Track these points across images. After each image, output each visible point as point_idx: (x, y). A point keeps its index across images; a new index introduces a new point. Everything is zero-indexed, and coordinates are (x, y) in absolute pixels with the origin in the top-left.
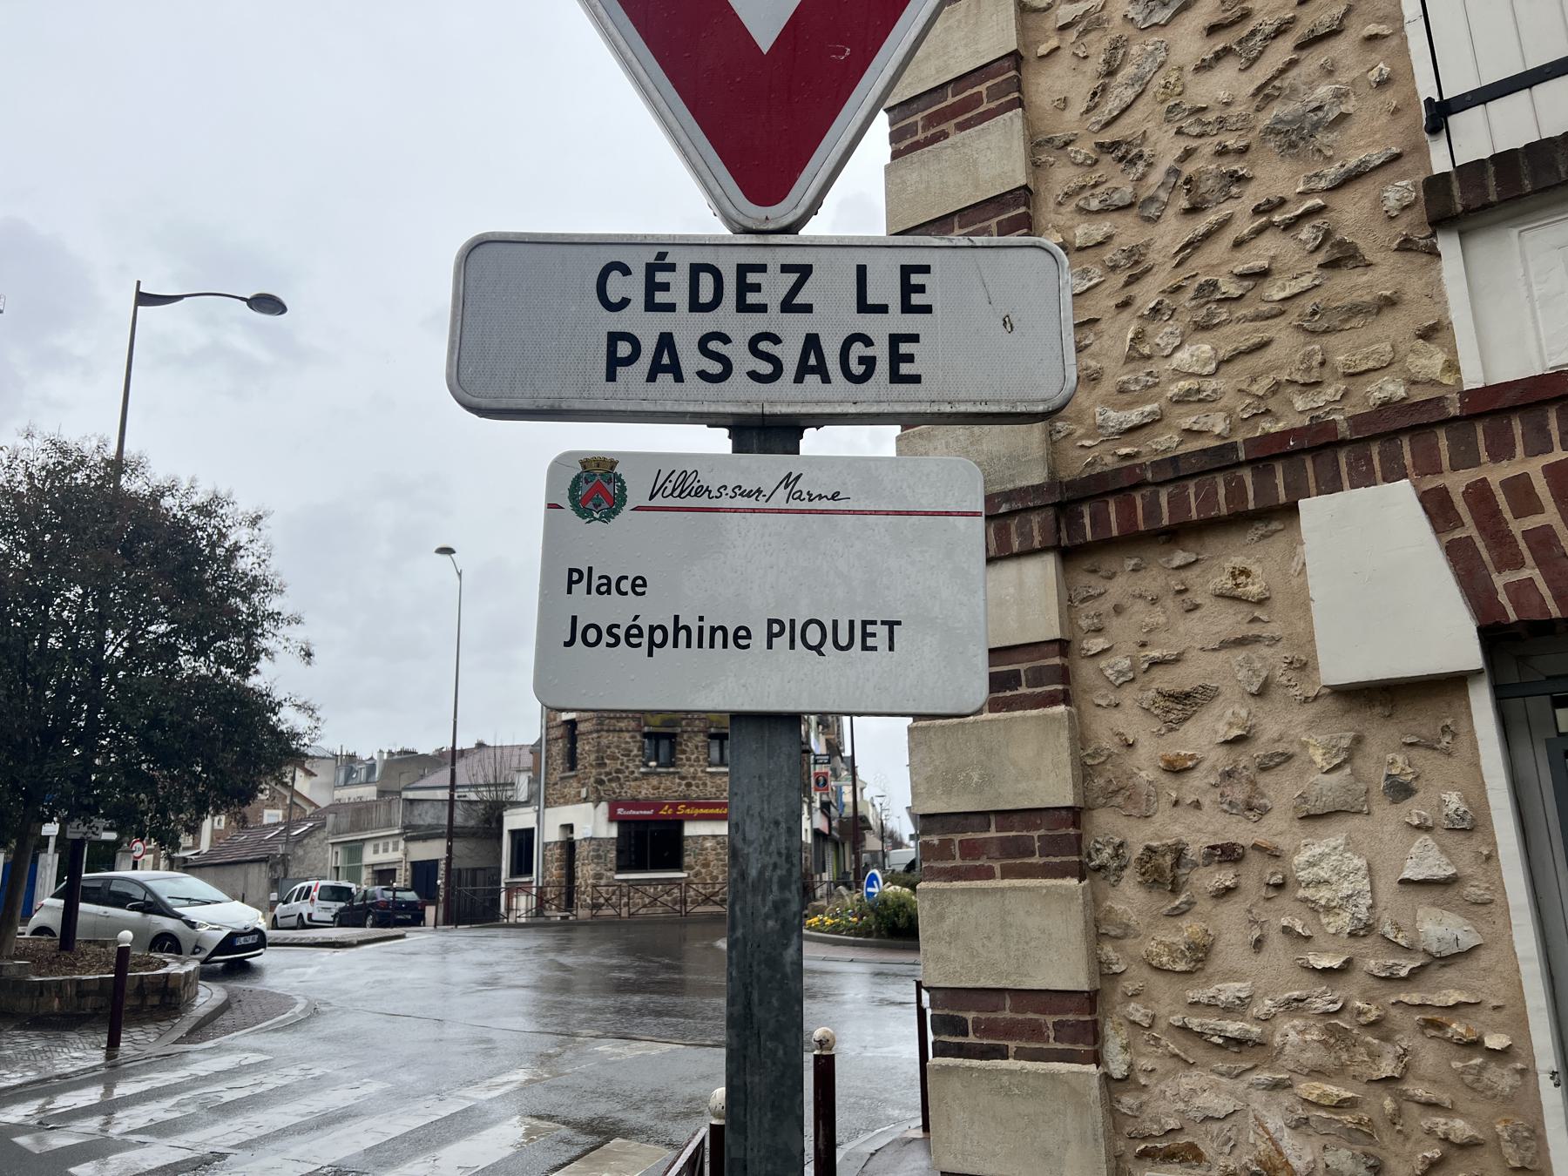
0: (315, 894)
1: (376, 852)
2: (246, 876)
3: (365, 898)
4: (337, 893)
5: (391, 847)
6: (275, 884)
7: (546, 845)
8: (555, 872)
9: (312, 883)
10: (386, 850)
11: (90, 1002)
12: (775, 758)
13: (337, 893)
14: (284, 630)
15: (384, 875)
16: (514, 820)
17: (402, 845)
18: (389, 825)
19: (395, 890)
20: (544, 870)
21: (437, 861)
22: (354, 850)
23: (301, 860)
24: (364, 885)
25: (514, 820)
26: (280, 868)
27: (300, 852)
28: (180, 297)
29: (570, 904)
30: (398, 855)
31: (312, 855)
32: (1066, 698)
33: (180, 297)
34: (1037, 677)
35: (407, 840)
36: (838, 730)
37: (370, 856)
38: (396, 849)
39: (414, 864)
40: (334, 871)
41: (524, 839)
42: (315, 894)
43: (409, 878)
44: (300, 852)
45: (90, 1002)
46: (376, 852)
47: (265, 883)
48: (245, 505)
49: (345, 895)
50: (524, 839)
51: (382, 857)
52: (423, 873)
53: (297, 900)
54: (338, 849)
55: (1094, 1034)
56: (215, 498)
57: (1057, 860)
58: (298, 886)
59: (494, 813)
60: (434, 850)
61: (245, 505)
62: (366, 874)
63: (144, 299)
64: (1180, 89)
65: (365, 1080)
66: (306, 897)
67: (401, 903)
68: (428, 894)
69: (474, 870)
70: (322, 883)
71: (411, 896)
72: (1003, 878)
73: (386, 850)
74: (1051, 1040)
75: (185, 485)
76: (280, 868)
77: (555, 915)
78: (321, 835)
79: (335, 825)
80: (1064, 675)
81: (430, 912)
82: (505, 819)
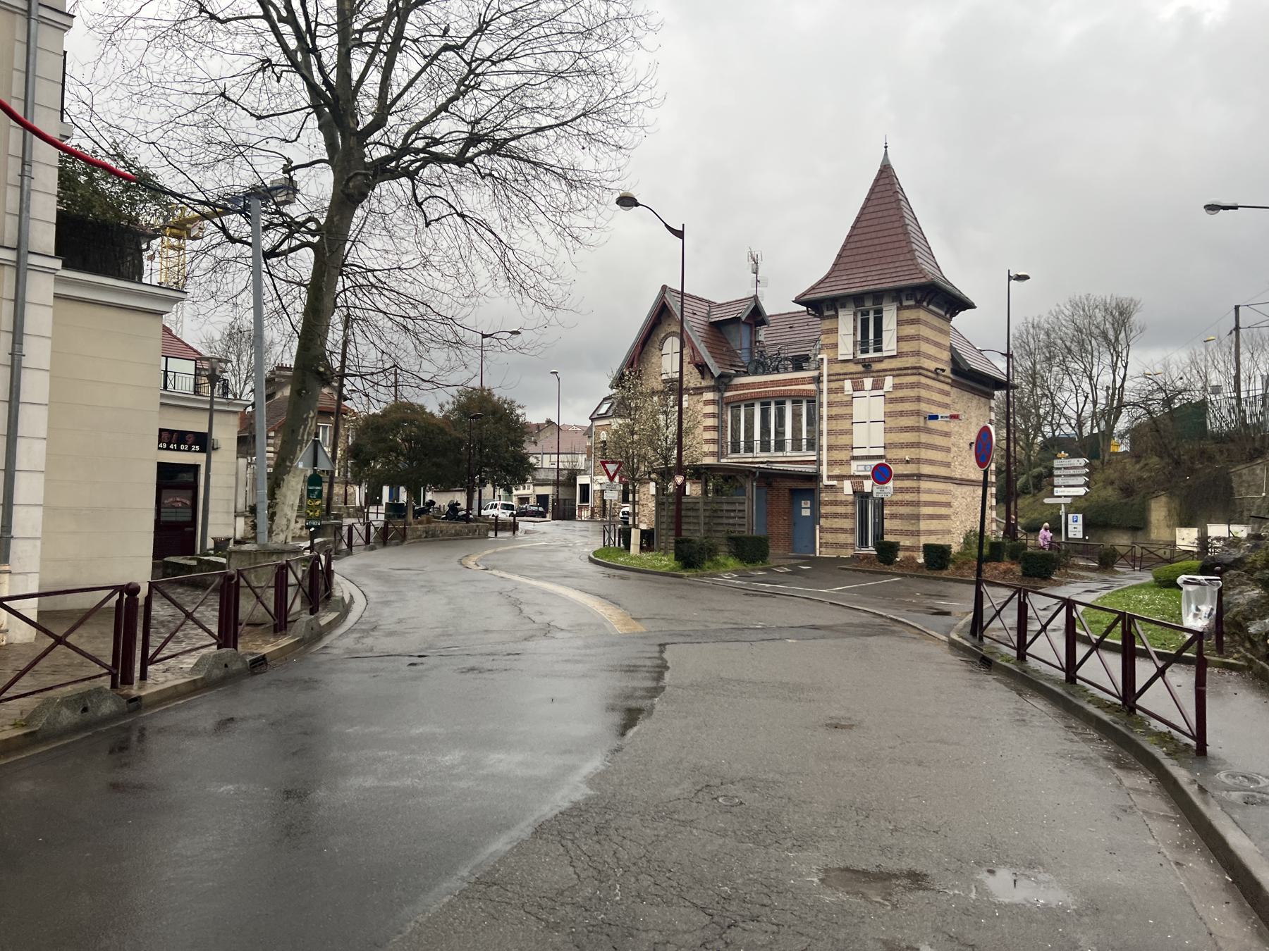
0: (499, 507)
1: (524, 489)
7: (595, 491)
8: (598, 502)
12: (149, 216)
16: (582, 480)
17: (532, 487)
20: (594, 501)
21: (548, 495)
25: (582, 480)
29: (604, 515)
30: (530, 491)
32: (780, 404)
35: (534, 485)
38: (529, 489)
39: (537, 496)
41: (585, 488)
42: (499, 507)
50: (585, 488)
52: (542, 499)
57: (742, 438)
59: (573, 474)
60: (547, 490)
62: (515, 499)
65: (549, 565)
66: (495, 507)
69: (565, 500)
72: (862, 319)
74: (742, 451)
77: (598, 517)
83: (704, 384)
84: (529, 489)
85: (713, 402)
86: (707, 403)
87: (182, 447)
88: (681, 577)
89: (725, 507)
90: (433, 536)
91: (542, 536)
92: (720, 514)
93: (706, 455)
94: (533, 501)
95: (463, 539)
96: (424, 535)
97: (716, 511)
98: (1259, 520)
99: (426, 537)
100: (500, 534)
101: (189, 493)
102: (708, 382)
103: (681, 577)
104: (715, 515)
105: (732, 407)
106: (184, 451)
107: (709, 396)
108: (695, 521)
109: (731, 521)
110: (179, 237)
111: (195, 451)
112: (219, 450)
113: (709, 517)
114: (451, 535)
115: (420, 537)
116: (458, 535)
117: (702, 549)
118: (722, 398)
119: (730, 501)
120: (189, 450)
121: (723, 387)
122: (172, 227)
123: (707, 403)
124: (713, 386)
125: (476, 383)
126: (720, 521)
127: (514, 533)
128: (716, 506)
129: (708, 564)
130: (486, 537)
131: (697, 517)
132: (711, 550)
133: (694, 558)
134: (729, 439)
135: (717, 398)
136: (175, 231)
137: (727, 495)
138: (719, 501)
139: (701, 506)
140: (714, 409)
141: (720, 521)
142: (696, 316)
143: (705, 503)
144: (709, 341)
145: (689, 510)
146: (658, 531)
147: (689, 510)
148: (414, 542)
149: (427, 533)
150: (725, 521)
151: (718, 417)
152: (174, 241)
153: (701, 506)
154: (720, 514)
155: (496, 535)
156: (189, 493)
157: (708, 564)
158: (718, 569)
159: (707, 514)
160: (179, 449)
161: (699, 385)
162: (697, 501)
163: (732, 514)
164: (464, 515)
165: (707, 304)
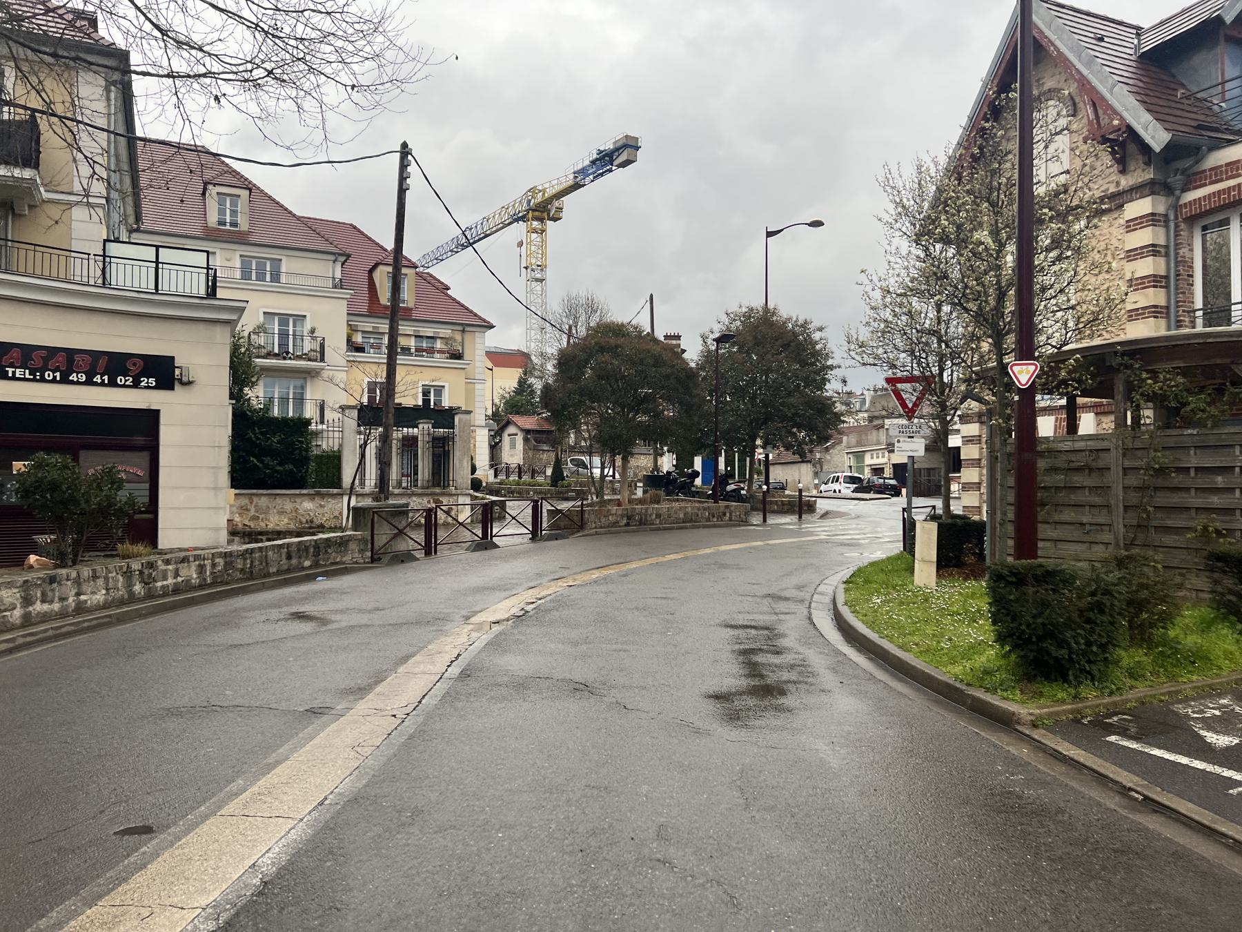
0: (841, 480)
1: (872, 458)
2: (799, 470)
3: (868, 482)
4: (852, 480)
5: (880, 455)
6: (816, 474)
9: (840, 474)
10: (878, 457)
11: (786, 507)
13: (852, 480)
14: (834, 372)
15: (878, 471)
18: (878, 443)
19: (885, 478)
22: (859, 456)
23: (829, 462)
24: (867, 474)
26: (818, 466)
27: (828, 457)
28: (782, 230)
30: (885, 460)
31: (835, 459)
33: (782, 230)
34: (977, 440)
36: (665, 529)
37: (868, 460)
38: (883, 457)
40: (849, 469)
42: (841, 480)
43: (892, 473)
44: (828, 457)
45: (786, 507)
46: (872, 458)
47: (811, 474)
48: (816, 324)
49: (857, 481)
51: (875, 461)
53: (832, 483)
54: (850, 456)
55: (980, 488)
56: (806, 322)
58: (832, 476)
61: (816, 324)
62: (867, 470)
63: (769, 234)
64: (1096, 272)
66: (837, 481)
67: (888, 485)
68: (903, 482)
70: (844, 474)
71: (893, 482)
73: (878, 457)
75: (794, 319)
76: (818, 466)
78: (838, 448)
79: (848, 443)
80: (980, 440)
81: (904, 491)
82: (949, 441)
83: (1126, 182)
84: (883, 457)
85: (1152, 219)
86: (1133, 225)
87: (120, 380)
88: (1004, 721)
89: (1194, 460)
90: (643, 522)
91: (856, 521)
92: (1176, 479)
93: (1135, 314)
94: (888, 472)
95: (698, 527)
96: (625, 521)
97: (1162, 471)
98: (273, 497)
99: (627, 525)
100: (773, 520)
101: (145, 457)
102: (1141, 174)
103: (1004, 721)
104: (1160, 482)
105: (1204, 228)
106: (124, 386)
107: (1140, 207)
108: (1097, 500)
109: (1215, 500)
110: (541, 220)
111: (148, 387)
112: (194, 389)
113: (1138, 489)
114: (677, 521)
115: (615, 524)
116: (691, 521)
117: (1099, 606)
118: (1176, 207)
119: (1212, 441)
120: (136, 385)
121: (1176, 180)
122: (534, 210)
123: (1133, 225)
124: (1152, 183)
125: (758, 303)
126: (1176, 499)
127: (800, 517)
128: (1164, 459)
129: (1128, 656)
130: (745, 522)
131: (1103, 489)
132: (1135, 605)
133: (1062, 644)
134: (1199, 303)
135: (1161, 209)
136: (537, 214)
137: (1200, 424)
138: (1172, 442)
139: (1113, 459)
140: (1155, 235)
141: (1176, 499)
142: (1103, 44)
143: (1126, 452)
144: (1140, 84)
145: (1079, 469)
146: (993, 528)
147: (1079, 469)
148: (597, 533)
149: (629, 518)
150: (1194, 500)
151: (1167, 255)
152: (535, 224)
153: (1113, 459)
154: (1176, 479)
155: (765, 521)
156: (145, 457)
157: (1128, 656)
158: (1172, 678)
159: (1133, 480)
160: (113, 384)
161: (1112, 189)
162: (1105, 444)
163: (1220, 480)
164: (734, 491)
165: (1135, 31)
